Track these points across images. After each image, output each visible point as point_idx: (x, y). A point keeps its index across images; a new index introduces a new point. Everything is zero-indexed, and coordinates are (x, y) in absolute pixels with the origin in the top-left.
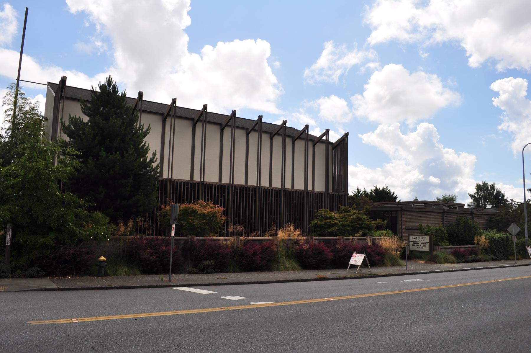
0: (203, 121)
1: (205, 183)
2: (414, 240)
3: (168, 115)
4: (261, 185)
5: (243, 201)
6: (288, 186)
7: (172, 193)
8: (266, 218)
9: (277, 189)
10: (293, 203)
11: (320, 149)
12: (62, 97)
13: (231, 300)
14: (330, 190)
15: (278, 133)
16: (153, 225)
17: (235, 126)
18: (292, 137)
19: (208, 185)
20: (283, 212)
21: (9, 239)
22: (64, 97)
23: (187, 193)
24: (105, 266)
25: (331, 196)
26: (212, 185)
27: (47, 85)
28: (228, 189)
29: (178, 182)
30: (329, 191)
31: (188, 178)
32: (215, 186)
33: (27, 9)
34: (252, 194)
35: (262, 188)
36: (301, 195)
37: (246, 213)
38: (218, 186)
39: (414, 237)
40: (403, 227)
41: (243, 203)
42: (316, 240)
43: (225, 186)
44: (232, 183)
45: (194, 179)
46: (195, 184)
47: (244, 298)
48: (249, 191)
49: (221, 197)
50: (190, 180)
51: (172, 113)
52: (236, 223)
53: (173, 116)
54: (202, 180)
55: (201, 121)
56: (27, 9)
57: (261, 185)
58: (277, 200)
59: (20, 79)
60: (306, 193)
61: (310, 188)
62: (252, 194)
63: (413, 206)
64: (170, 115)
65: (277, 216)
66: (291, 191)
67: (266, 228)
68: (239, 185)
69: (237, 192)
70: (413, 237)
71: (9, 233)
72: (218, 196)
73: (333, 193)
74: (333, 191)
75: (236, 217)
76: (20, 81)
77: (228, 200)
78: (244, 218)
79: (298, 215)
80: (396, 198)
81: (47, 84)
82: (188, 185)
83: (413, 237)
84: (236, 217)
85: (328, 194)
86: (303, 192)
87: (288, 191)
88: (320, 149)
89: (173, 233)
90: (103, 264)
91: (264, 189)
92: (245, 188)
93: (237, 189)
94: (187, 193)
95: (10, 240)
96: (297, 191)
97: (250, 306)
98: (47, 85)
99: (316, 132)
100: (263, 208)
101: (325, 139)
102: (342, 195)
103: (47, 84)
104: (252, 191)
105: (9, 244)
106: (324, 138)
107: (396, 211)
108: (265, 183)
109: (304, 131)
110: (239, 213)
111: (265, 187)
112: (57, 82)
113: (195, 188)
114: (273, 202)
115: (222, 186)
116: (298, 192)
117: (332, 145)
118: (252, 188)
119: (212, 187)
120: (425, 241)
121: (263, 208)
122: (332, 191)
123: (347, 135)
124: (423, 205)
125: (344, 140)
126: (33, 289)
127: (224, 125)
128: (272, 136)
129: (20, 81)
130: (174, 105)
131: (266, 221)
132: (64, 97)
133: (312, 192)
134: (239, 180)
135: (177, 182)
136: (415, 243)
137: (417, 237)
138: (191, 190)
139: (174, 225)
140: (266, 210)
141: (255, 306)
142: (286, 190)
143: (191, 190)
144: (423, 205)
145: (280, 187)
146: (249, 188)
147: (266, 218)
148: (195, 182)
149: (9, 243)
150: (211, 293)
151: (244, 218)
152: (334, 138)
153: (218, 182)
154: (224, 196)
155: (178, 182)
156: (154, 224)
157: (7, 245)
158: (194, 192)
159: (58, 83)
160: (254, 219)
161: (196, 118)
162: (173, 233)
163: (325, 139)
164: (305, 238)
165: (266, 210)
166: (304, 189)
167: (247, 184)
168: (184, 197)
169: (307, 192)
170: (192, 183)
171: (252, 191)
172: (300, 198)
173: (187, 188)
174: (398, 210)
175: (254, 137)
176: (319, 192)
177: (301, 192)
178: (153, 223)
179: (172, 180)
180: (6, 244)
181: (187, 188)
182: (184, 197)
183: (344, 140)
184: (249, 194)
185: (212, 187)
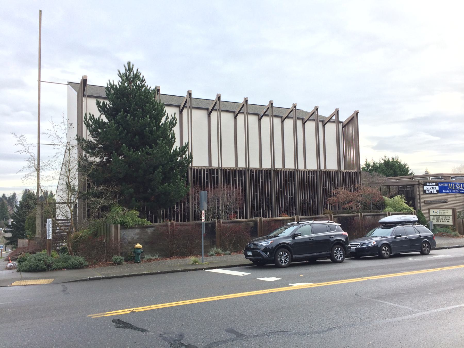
0: (217, 110)
1: (223, 168)
2: (435, 214)
3: (213, 109)
4: (276, 167)
5: (259, 183)
6: (301, 167)
7: (193, 180)
8: (281, 199)
9: (291, 170)
10: (307, 183)
11: (331, 128)
12: (84, 96)
13: (269, 282)
14: (342, 168)
15: (289, 116)
16: (178, 210)
17: (248, 112)
18: (322, 121)
19: (226, 170)
20: (298, 192)
21: (50, 233)
22: (87, 96)
23: (207, 179)
24: (141, 253)
25: (344, 174)
26: (230, 170)
27: (67, 85)
28: (245, 172)
29: (198, 169)
30: (342, 169)
31: (207, 165)
32: (232, 170)
33: (40, 11)
34: (267, 176)
35: (276, 170)
36: (314, 174)
37: (262, 195)
38: (235, 170)
39: (435, 210)
40: (422, 200)
41: (259, 185)
42: (335, 218)
43: (241, 170)
44: (248, 167)
45: (327, 168)
46: (214, 170)
47: (280, 279)
48: (265, 174)
49: (239, 181)
50: (208, 166)
51: (188, 104)
52: (282, 212)
53: (190, 107)
54: (220, 166)
55: (216, 110)
56: (40, 11)
57: (276, 167)
58: (291, 180)
59: (41, 80)
60: (319, 172)
61: (322, 168)
62: (267, 176)
63: (430, 179)
64: (187, 107)
65: (292, 195)
66: (304, 172)
67: (282, 208)
68: (255, 168)
69: (253, 175)
70: (434, 211)
71: (49, 228)
72: (236, 180)
73: (345, 171)
74: (345, 169)
75: (254, 199)
76: (41, 82)
77: (245, 183)
78: (261, 199)
79: (312, 194)
80: (408, 171)
81: (67, 84)
82: (207, 171)
83: (434, 211)
84: (254, 199)
85: (340, 172)
86: (316, 172)
87: (301, 171)
88: (331, 128)
89: (203, 218)
90: (139, 251)
91: (278, 171)
92: (261, 170)
93: (253, 172)
94: (207, 179)
95: (50, 234)
96: (310, 170)
97: (291, 287)
98: (67, 85)
99: (325, 113)
100: (279, 189)
101: (335, 119)
102: (354, 172)
103: (67, 83)
104: (267, 174)
105: (50, 238)
106: (334, 118)
107: (413, 186)
108: (279, 166)
109: (314, 112)
110: (257, 195)
111: (279, 169)
112: (79, 82)
113: (214, 174)
114: (283, 182)
115: (239, 170)
116: (311, 172)
117: (342, 124)
118: (267, 171)
119: (229, 172)
120: (447, 214)
121: (279, 189)
122: (344, 169)
123: (357, 113)
124: (441, 177)
125: (354, 119)
126: (78, 280)
127: (237, 112)
128: (283, 119)
129: (41, 82)
130: (190, 97)
131: (282, 201)
132: (87, 96)
133: (325, 171)
134: (254, 165)
135: (197, 170)
136: (436, 216)
137: (438, 210)
138: (211, 176)
139: (204, 211)
140: (281, 191)
141: (295, 287)
142: (300, 170)
143: (211, 176)
144: (441, 177)
145: (294, 168)
146: (265, 171)
147: (281, 199)
148: (214, 168)
149: (50, 237)
150: (246, 274)
151: (261, 199)
152: (343, 117)
153: (234, 166)
154: (242, 180)
155: (198, 169)
156: (178, 210)
157: (49, 240)
158: (214, 177)
159: (79, 82)
160: (271, 200)
161: (306, 118)
162: (203, 218)
163: (335, 119)
164: (98, 160)
165: (281, 191)
166: (218, 166)
167: (262, 167)
168: (204, 182)
169: (320, 172)
170: (211, 169)
171: (267, 174)
172: (314, 177)
173: (207, 174)
174: (415, 184)
175: (266, 121)
176: (332, 171)
177: (314, 172)
178: (178, 208)
179: (193, 168)
180: (47, 238)
181: (207, 174)
182: (204, 182)
183: (354, 119)
184: (265, 176)
185: (229, 172)
